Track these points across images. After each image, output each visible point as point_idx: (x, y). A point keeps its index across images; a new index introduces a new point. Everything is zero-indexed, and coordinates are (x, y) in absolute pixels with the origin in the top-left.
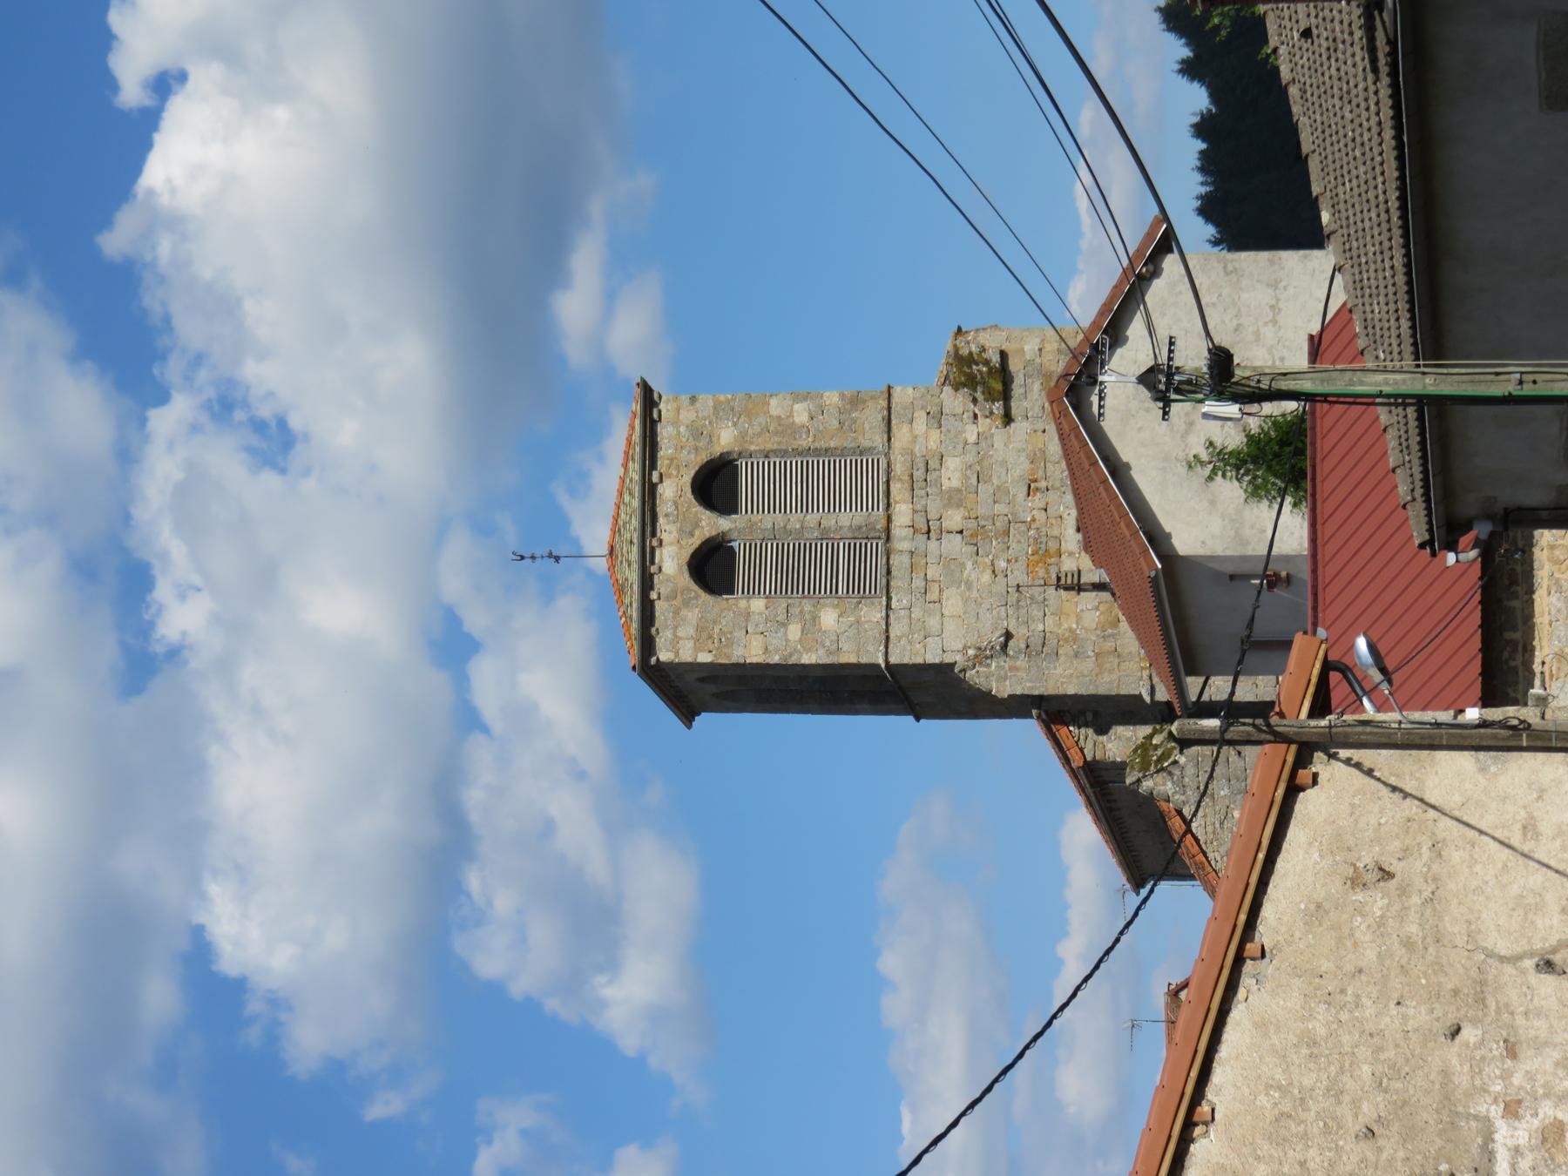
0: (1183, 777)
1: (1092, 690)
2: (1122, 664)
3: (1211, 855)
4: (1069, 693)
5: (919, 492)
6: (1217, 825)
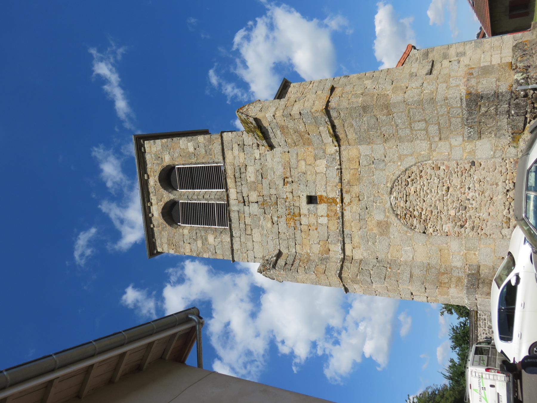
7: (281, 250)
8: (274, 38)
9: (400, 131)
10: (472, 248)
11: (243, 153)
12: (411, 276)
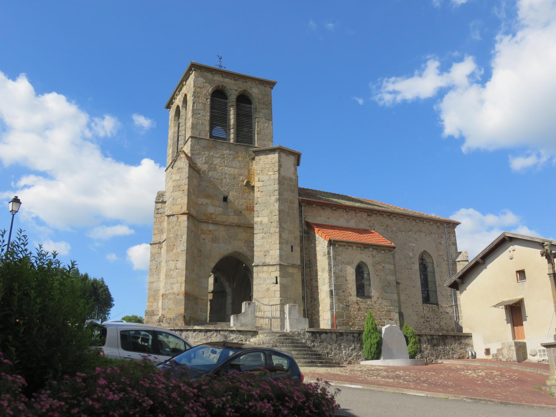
7: (167, 202)
9: (173, 262)
11: (441, 324)
12: (151, 283)
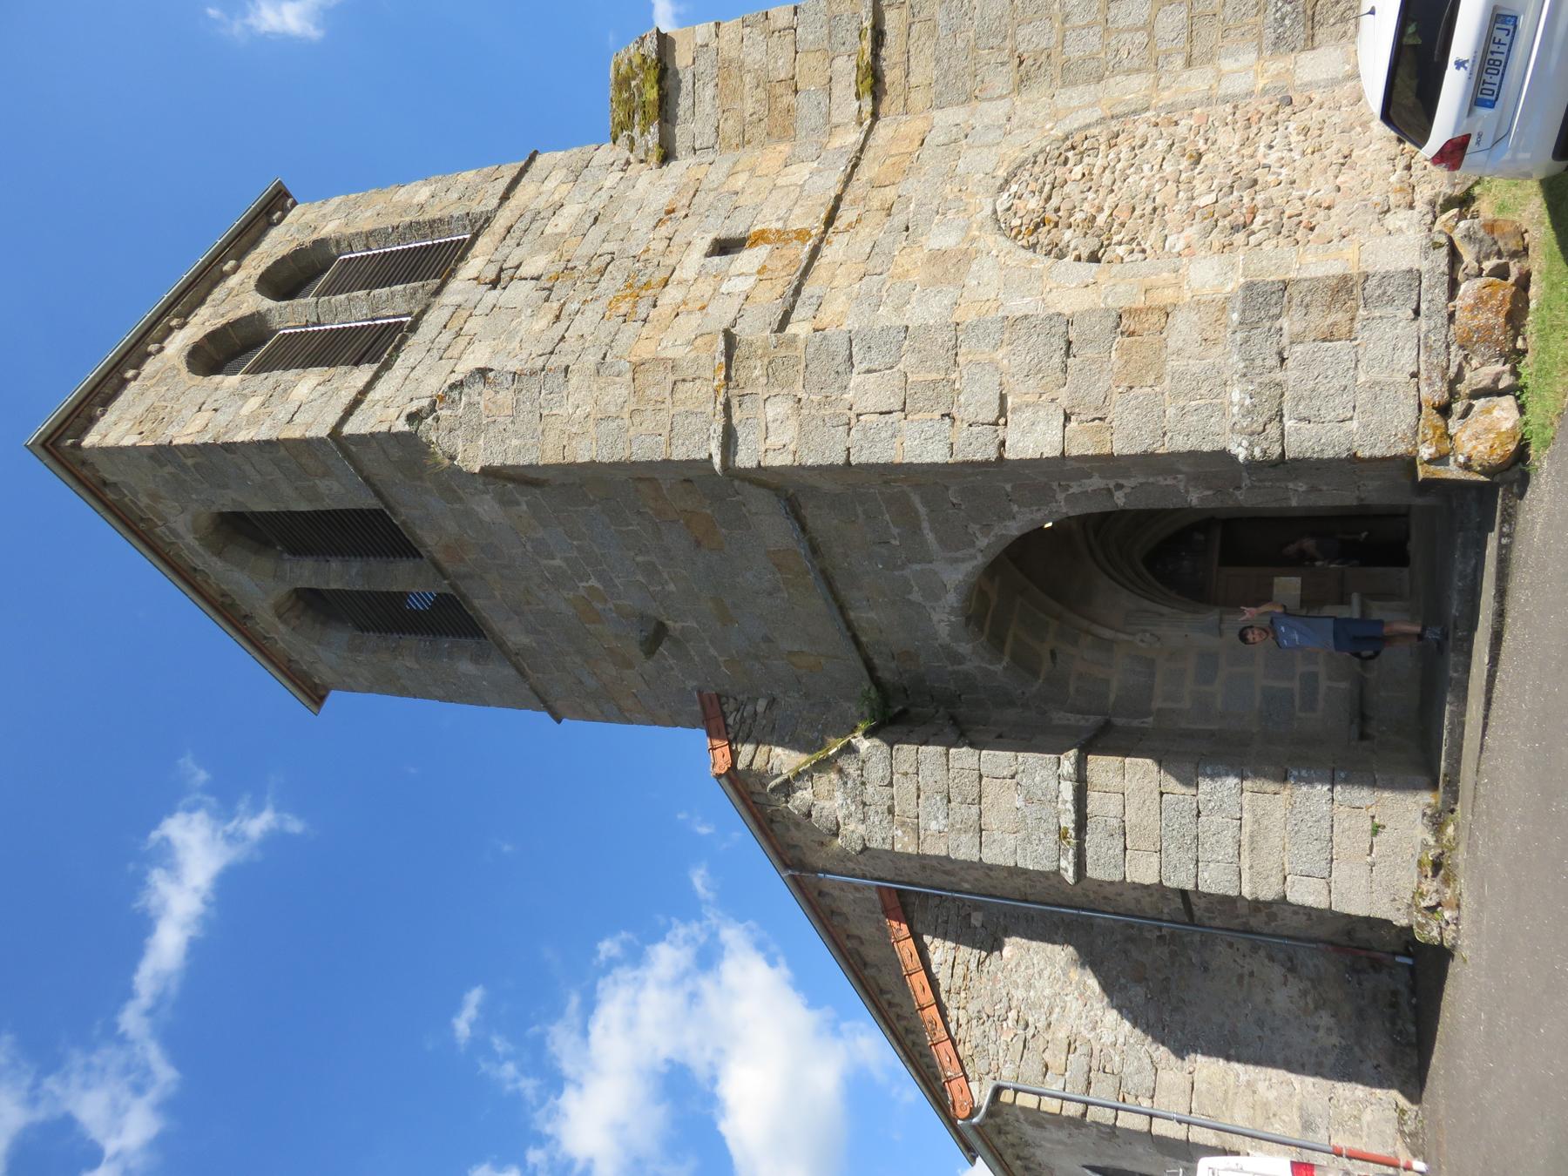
0: (863, 783)
1: (620, 454)
2: (679, 385)
3: (952, 1014)
4: (580, 460)
5: (510, 241)
6: (973, 966)
8: (694, 997)
10: (1273, 268)
